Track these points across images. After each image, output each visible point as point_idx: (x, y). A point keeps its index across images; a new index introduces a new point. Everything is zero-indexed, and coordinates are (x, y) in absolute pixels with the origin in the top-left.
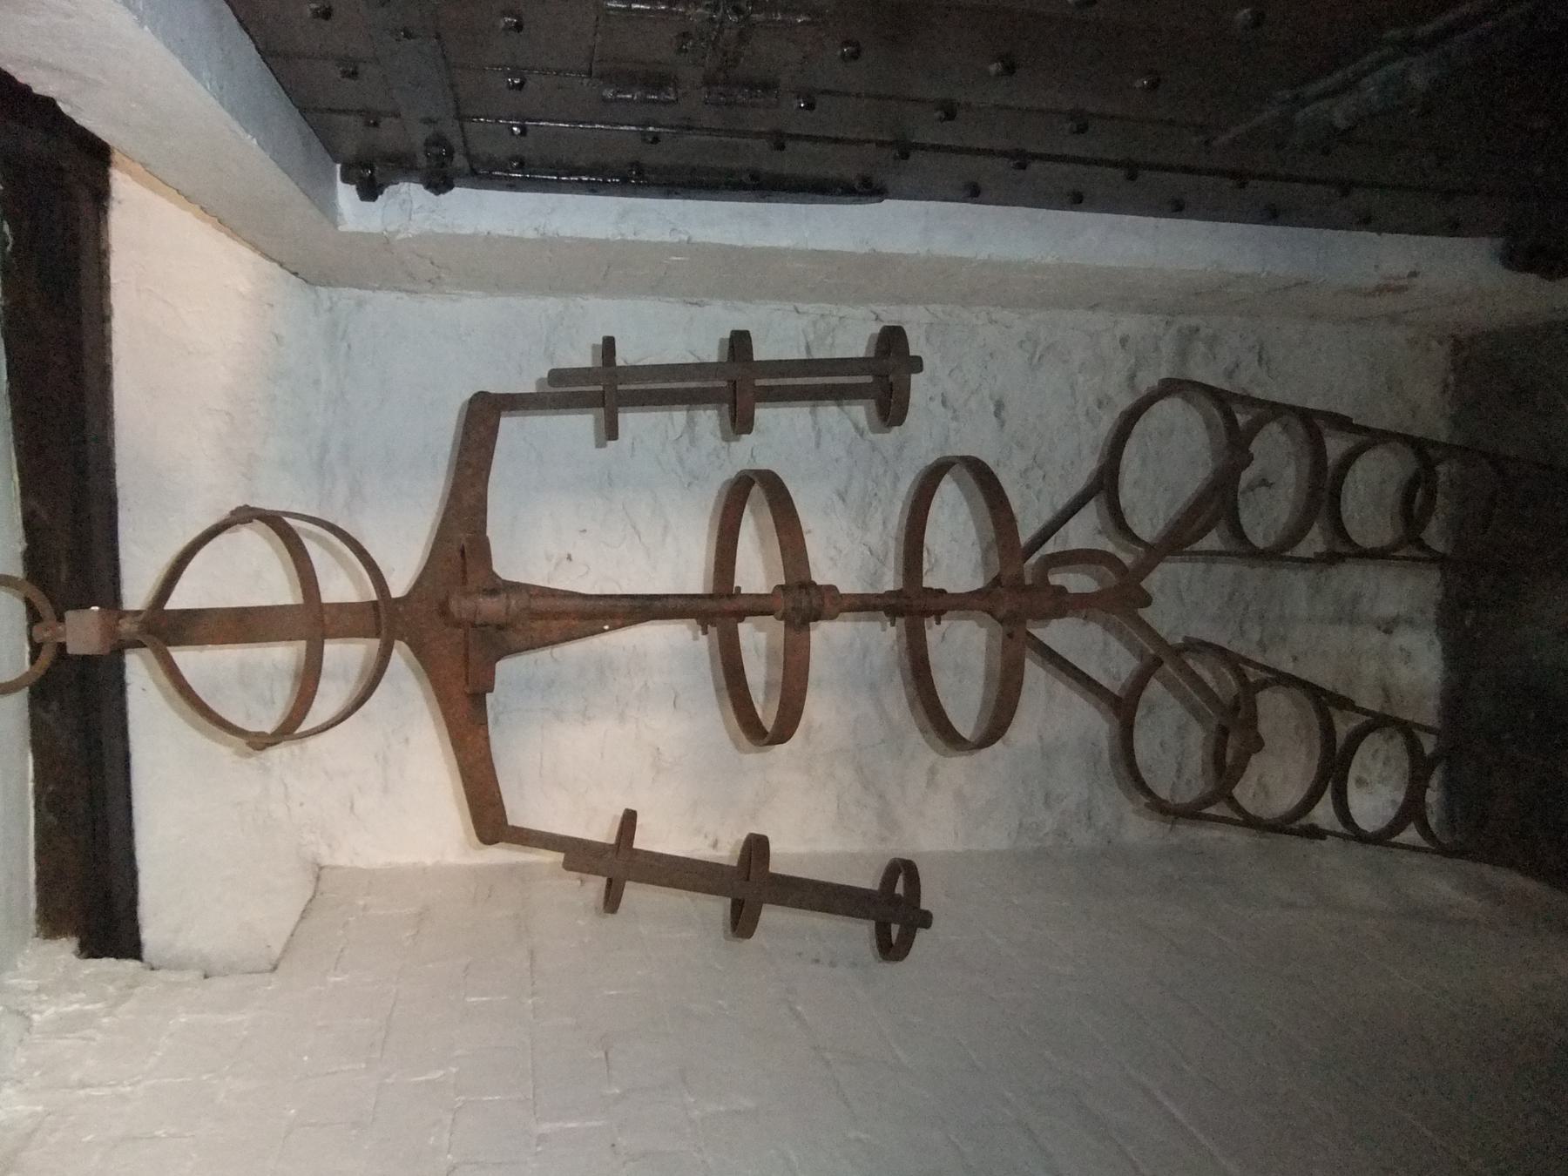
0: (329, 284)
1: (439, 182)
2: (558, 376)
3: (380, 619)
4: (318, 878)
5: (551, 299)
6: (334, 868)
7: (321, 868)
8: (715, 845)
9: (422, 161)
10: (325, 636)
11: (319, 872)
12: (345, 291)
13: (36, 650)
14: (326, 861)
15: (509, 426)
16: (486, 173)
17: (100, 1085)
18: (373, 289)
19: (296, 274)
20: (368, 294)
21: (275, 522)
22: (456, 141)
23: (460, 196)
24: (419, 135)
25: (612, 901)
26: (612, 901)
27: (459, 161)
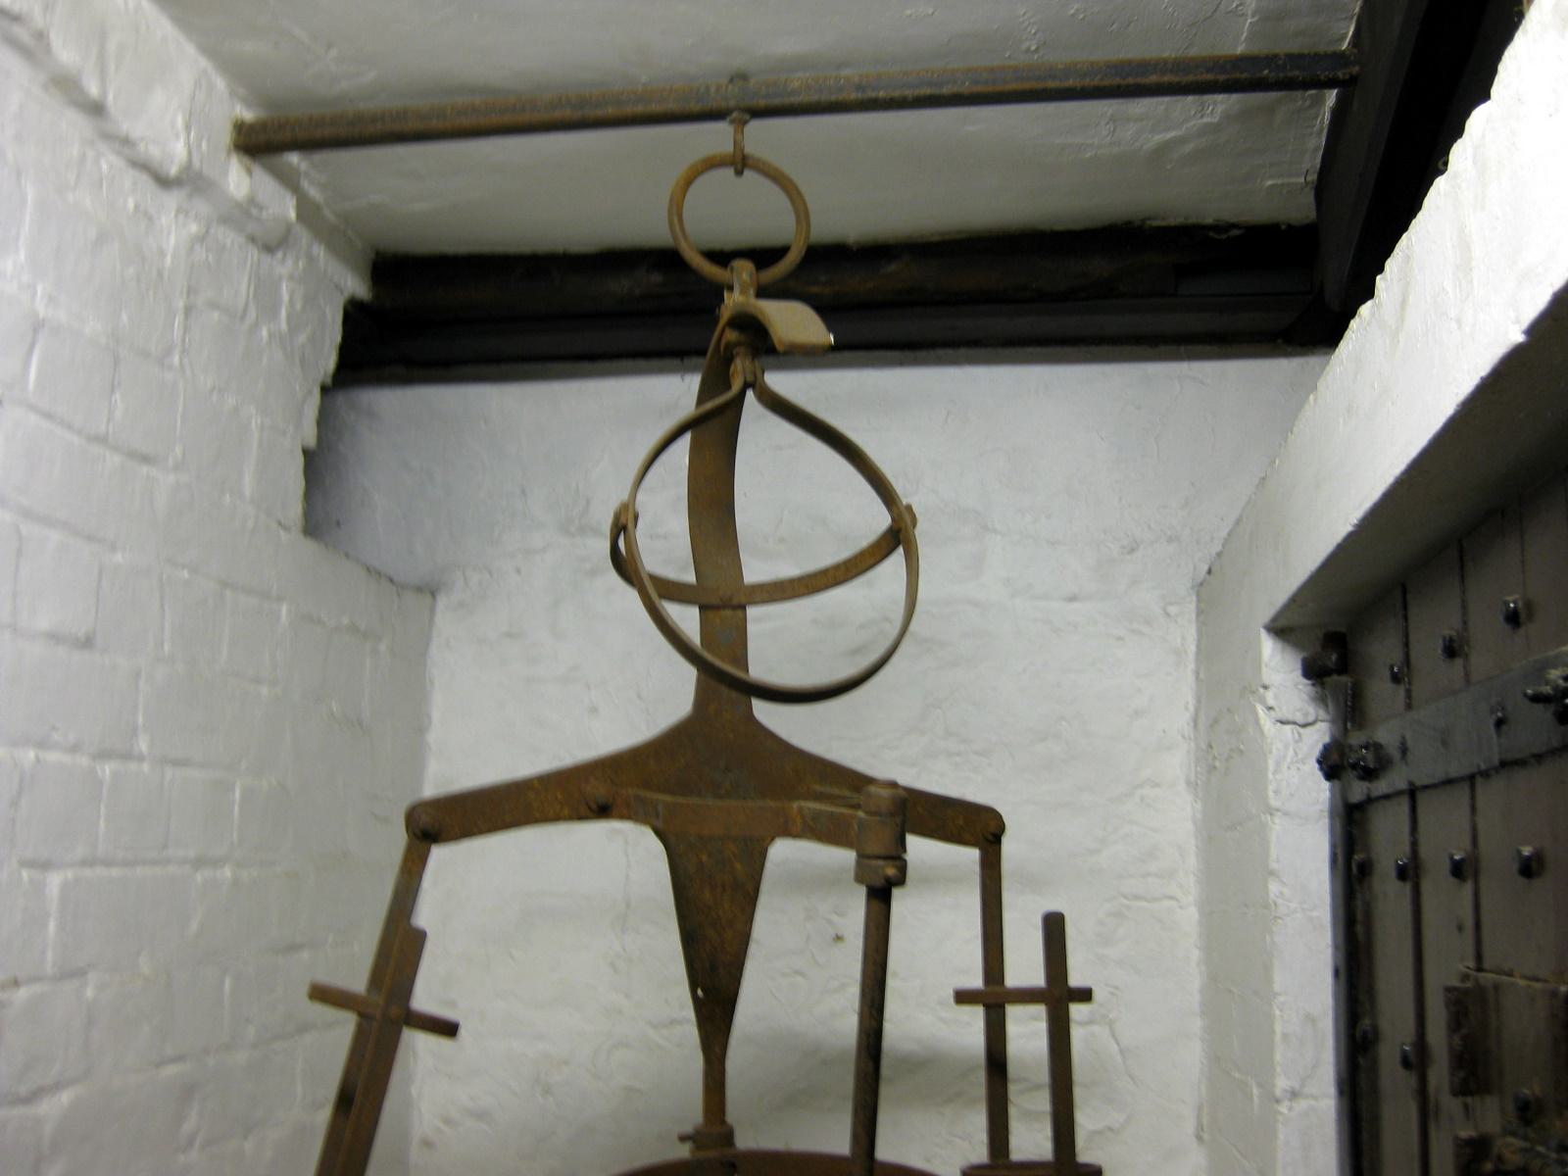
0: (1200, 612)
1: (1333, 764)
2: (419, 938)
3: (725, 681)
4: (419, 589)
5: (1196, 916)
6: (432, 611)
7: (433, 595)
8: (427, 1144)
9: (1356, 738)
10: (703, 608)
11: (430, 590)
12: (1192, 632)
13: (721, 257)
14: (442, 601)
15: (971, 855)
16: (1351, 826)
17: (186, 329)
18: (1197, 673)
19: (1209, 572)
20: (1192, 666)
21: (898, 537)
22: (1381, 786)
23: (1321, 790)
24: (1386, 734)
25: (963, 997)
26: (963, 997)
27: (1358, 790)
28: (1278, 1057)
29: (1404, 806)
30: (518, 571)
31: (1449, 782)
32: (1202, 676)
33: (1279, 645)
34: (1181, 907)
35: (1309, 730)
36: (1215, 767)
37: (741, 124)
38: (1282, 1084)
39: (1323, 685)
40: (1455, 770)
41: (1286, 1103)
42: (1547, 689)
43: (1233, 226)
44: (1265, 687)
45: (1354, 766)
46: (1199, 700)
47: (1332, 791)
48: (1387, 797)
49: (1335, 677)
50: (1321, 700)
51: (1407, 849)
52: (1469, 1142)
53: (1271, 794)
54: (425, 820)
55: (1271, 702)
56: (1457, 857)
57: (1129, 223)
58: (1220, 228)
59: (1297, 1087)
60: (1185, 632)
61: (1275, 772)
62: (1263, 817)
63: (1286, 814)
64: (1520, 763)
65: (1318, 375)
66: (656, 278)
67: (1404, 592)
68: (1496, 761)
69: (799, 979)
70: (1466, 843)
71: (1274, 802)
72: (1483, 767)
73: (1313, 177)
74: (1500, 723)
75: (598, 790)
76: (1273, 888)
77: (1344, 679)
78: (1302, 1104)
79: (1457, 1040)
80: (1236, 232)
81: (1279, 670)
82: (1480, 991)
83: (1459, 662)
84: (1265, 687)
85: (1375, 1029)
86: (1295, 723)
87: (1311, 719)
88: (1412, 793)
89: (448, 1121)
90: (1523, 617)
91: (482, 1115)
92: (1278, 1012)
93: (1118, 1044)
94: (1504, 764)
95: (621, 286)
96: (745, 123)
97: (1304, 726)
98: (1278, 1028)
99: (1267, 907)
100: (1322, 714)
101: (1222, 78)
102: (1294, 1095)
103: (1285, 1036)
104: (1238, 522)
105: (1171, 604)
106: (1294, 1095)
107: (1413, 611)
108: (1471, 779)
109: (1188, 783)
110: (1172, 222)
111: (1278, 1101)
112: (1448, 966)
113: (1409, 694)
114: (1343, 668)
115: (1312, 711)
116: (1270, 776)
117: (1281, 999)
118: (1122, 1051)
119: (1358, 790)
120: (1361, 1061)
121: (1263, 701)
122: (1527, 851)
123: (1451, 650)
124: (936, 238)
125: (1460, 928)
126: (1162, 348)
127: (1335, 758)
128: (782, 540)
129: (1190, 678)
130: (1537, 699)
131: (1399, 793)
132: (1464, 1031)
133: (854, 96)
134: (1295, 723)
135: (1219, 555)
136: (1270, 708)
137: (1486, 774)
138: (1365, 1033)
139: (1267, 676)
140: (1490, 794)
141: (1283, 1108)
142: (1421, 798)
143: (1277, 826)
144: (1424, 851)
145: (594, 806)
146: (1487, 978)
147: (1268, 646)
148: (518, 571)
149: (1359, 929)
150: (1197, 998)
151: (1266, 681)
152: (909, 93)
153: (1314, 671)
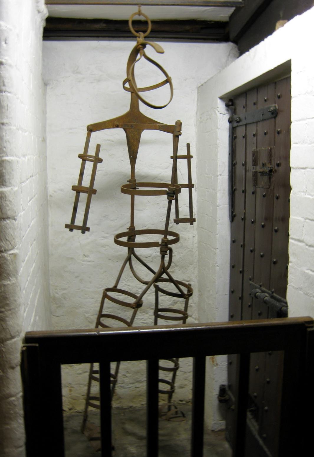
0: (198, 93)
1: (230, 121)
8: (51, 196)
9: (235, 116)
18: (197, 105)
20: (196, 103)
23: (228, 124)
24: (242, 116)
28: (218, 169)
29: (244, 127)
30: (64, 81)
31: (253, 123)
32: (198, 105)
33: (221, 101)
34: (193, 148)
35: (225, 115)
36: (202, 122)
37: (140, 6)
38: (219, 173)
39: (229, 108)
40: (254, 121)
41: (219, 176)
42: (270, 110)
43: (212, 21)
44: (218, 108)
45: (236, 121)
46: (198, 109)
47: (230, 125)
48: (241, 126)
49: (231, 107)
50: (228, 110)
51: (244, 133)
52: (254, 172)
53: (218, 126)
54: (91, 128)
55: (219, 110)
56: (254, 133)
57: (194, 19)
58: (210, 21)
59: (221, 174)
60: (195, 96)
61: (219, 122)
62: (216, 130)
63: (221, 129)
64: (265, 120)
65: (235, 59)
66: (104, 25)
67: (246, 94)
68: (262, 119)
69: (122, 162)
70: (255, 131)
71: (219, 127)
72: (259, 120)
73: (230, 15)
74: (263, 115)
75: (117, 123)
76: (218, 141)
77: (233, 107)
78: (222, 177)
79: (253, 158)
80: (213, 22)
81: (221, 106)
82: (257, 152)
83: (256, 106)
84: (218, 108)
85: (236, 162)
86: (222, 114)
87: (225, 113)
88: (246, 125)
89: (55, 192)
90: (267, 100)
91: (61, 190)
92: (218, 162)
93: (181, 173)
94: (263, 120)
95: (97, 26)
96: (141, 6)
97: (224, 114)
98: (218, 164)
99: (217, 145)
100: (227, 113)
101: (222, 5)
102: (220, 175)
103: (219, 166)
104: (212, 78)
105: (192, 91)
106: (220, 175)
107: (247, 95)
108: (257, 122)
109: (195, 125)
110: (202, 20)
111: (218, 176)
112: (251, 148)
113: (246, 110)
114: (232, 105)
115: (226, 112)
116: (218, 123)
117: (219, 159)
118: (182, 175)
119: (235, 124)
120: (234, 168)
121: (217, 110)
122: (265, 131)
123: (255, 104)
124: (159, 20)
125: (254, 144)
126: (193, 40)
127: (231, 120)
128: (118, 76)
129: (196, 105)
130: (270, 111)
131: (244, 125)
132: (255, 157)
133: (161, 3)
134: (222, 114)
135: (206, 82)
136: (219, 111)
137: (259, 121)
138: (235, 163)
139: (219, 106)
140: (260, 124)
141: (219, 177)
142: (247, 126)
143: (219, 131)
144: (247, 133)
145: (116, 126)
146: (258, 149)
147: (219, 101)
148: (64, 81)
149: (234, 147)
150: (195, 165)
151: (218, 107)
152: (170, 4)
153: (227, 105)
